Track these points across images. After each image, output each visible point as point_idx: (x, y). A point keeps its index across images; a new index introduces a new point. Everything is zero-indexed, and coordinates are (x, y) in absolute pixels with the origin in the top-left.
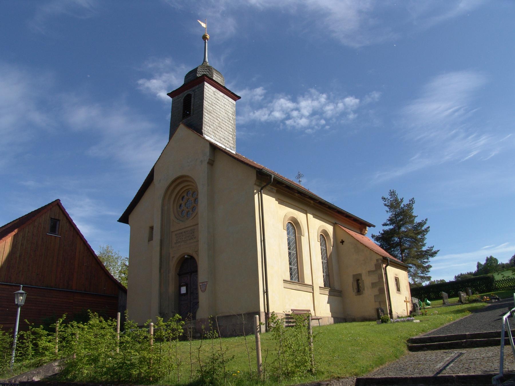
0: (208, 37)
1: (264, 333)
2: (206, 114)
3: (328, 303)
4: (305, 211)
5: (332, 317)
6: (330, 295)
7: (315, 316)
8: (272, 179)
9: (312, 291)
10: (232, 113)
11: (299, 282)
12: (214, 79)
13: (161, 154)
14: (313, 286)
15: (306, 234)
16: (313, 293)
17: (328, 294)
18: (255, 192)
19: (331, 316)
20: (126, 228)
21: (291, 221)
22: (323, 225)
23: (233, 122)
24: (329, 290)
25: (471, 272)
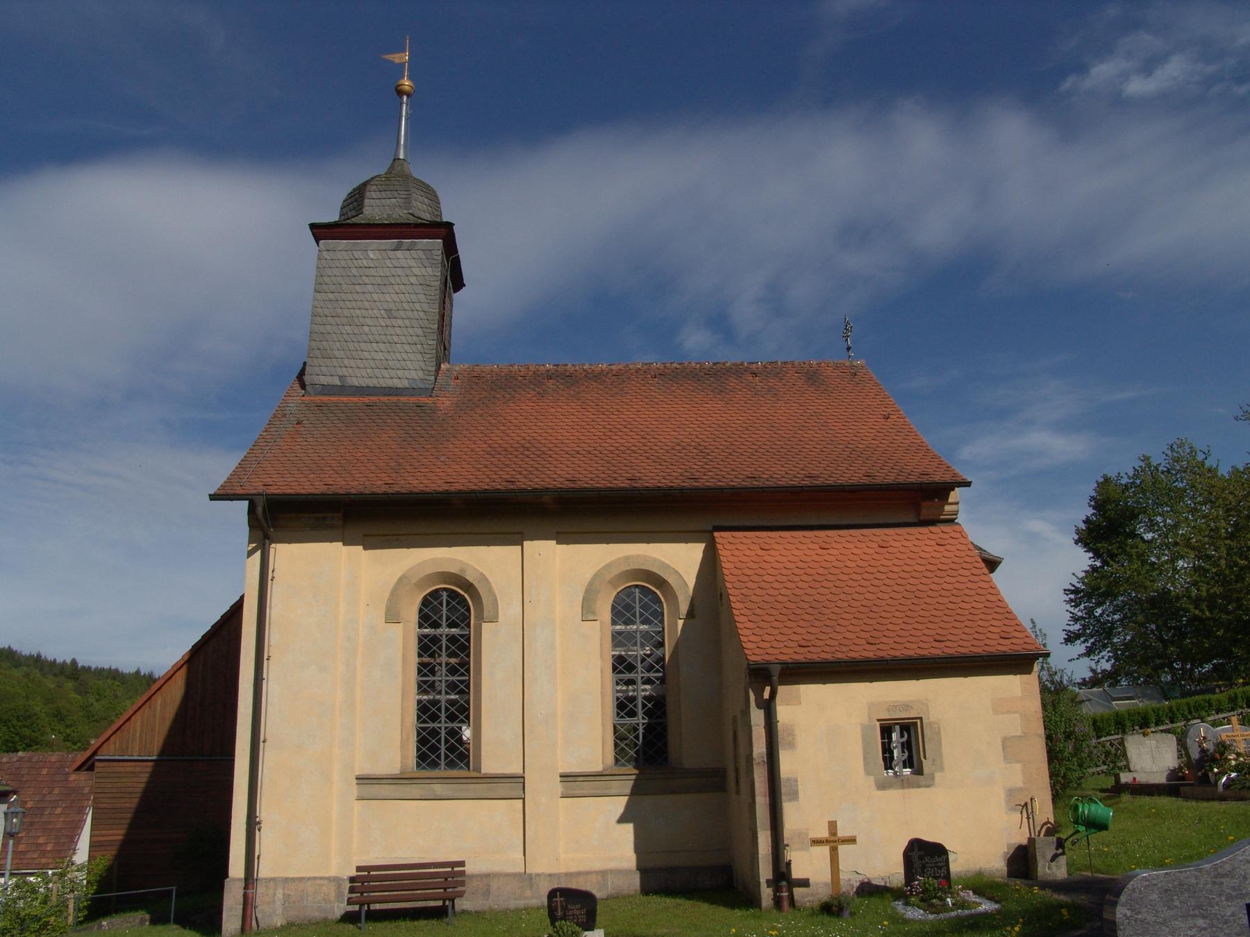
6: (635, 792)
16: (524, 799)
19: (635, 869)
22: (627, 558)
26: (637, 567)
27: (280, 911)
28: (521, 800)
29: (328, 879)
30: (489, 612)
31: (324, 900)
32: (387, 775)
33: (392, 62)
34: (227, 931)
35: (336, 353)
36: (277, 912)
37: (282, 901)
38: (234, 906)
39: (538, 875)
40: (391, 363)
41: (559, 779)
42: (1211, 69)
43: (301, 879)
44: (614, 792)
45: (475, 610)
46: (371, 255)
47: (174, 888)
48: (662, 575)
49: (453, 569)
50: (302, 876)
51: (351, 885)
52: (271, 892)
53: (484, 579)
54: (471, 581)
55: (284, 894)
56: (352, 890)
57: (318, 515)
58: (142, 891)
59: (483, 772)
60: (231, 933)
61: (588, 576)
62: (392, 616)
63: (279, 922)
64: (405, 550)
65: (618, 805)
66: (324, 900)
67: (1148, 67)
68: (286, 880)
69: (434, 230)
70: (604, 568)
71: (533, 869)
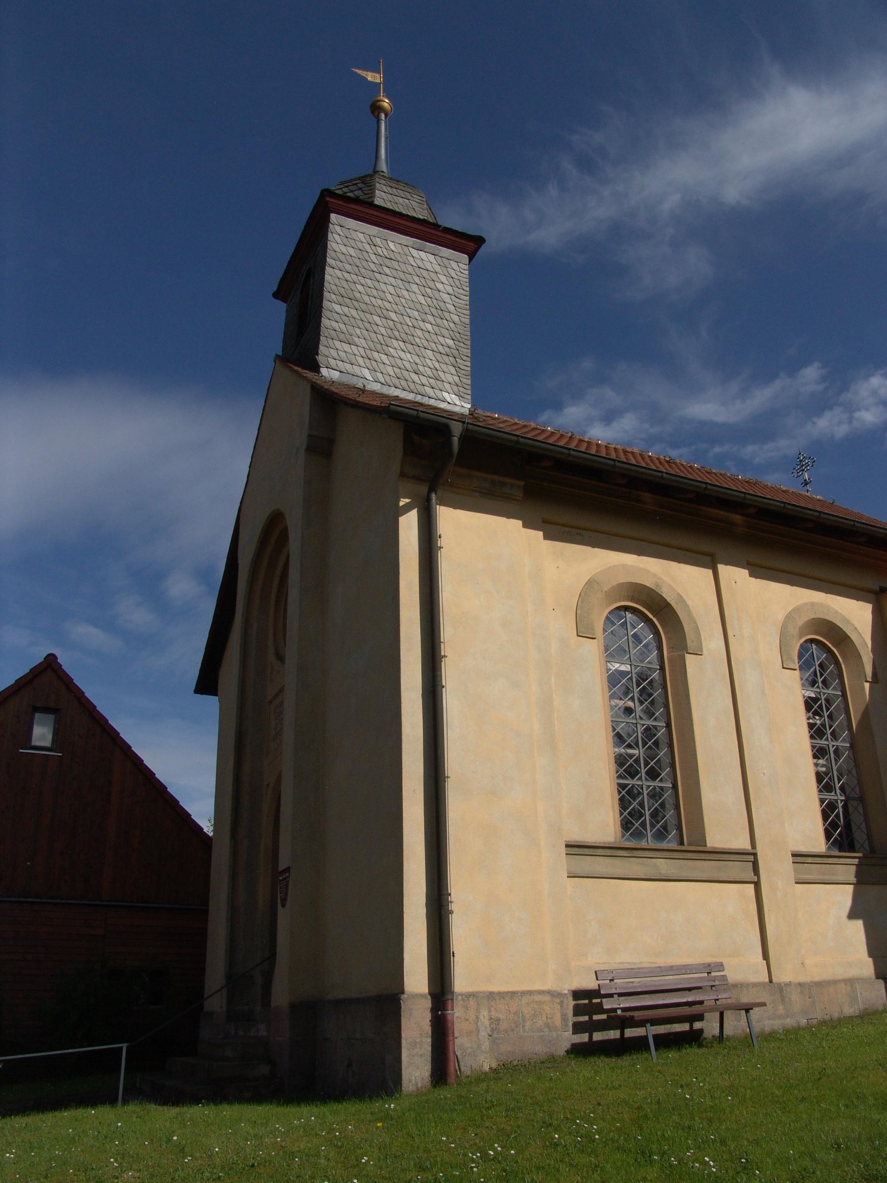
0: (386, 104)
1: (418, 1093)
2: (337, 308)
3: (852, 915)
4: (708, 559)
5: (878, 977)
6: (862, 881)
7: (771, 981)
8: (455, 440)
9: (751, 876)
10: (451, 292)
11: (682, 843)
12: (378, 202)
13: (248, 469)
14: (755, 855)
15: (713, 643)
16: (757, 885)
17: (854, 880)
18: (401, 504)
19: (873, 976)
20: (211, 703)
21: (633, 599)
22: (812, 605)
23: (456, 318)
24: (856, 861)
25: (287, 1105)
26: (822, 617)
27: (486, 1045)
28: (752, 886)
29: (549, 992)
30: (692, 642)
31: (547, 1025)
32: (605, 843)
33: (365, 79)
34: (410, 1080)
35: (356, 339)
36: (483, 1047)
37: (489, 1029)
38: (418, 1040)
39: (789, 984)
40: (421, 368)
41: (791, 859)
42: (655, 430)
43: (513, 994)
44: (841, 878)
45: (668, 639)
46: (392, 246)
47: (124, 1046)
48: (845, 629)
49: (649, 583)
50: (511, 989)
51: (575, 1002)
52: (472, 1016)
53: (680, 598)
54: (668, 601)
55: (491, 1019)
56: (577, 1011)
57: (495, 477)
58: (70, 1051)
59: (708, 845)
60: (416, 1084)
61: (781, 617)
62: (583, 632)
63: (487, 1063)
64: (589, 548)
65: (844, 896)
66: (547, 1025)
67: (608, 418)
68: (491, 996)
69: (463, 242)
70: (793, 610)
71: (785, 974)
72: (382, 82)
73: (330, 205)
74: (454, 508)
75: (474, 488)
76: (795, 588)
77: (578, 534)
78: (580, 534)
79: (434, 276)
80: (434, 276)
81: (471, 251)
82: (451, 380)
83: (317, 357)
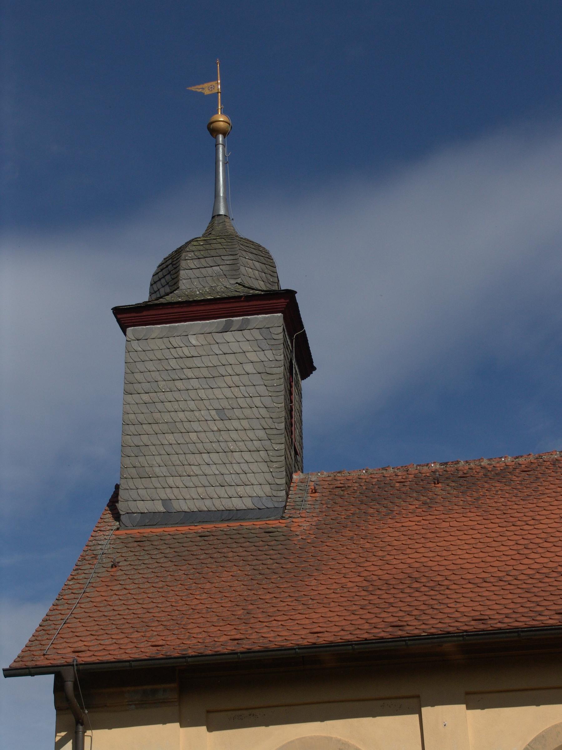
72: (219, 91)
73: (123, 322)
74: (109, 729)
75: (127, 703)
76: (542, 707)
77: (250, 715)
78: (253, 715)
79: (241, 358)
80: (241, 358)
81: (283, 308)
82: (262, 481)
83: (117, 504)
